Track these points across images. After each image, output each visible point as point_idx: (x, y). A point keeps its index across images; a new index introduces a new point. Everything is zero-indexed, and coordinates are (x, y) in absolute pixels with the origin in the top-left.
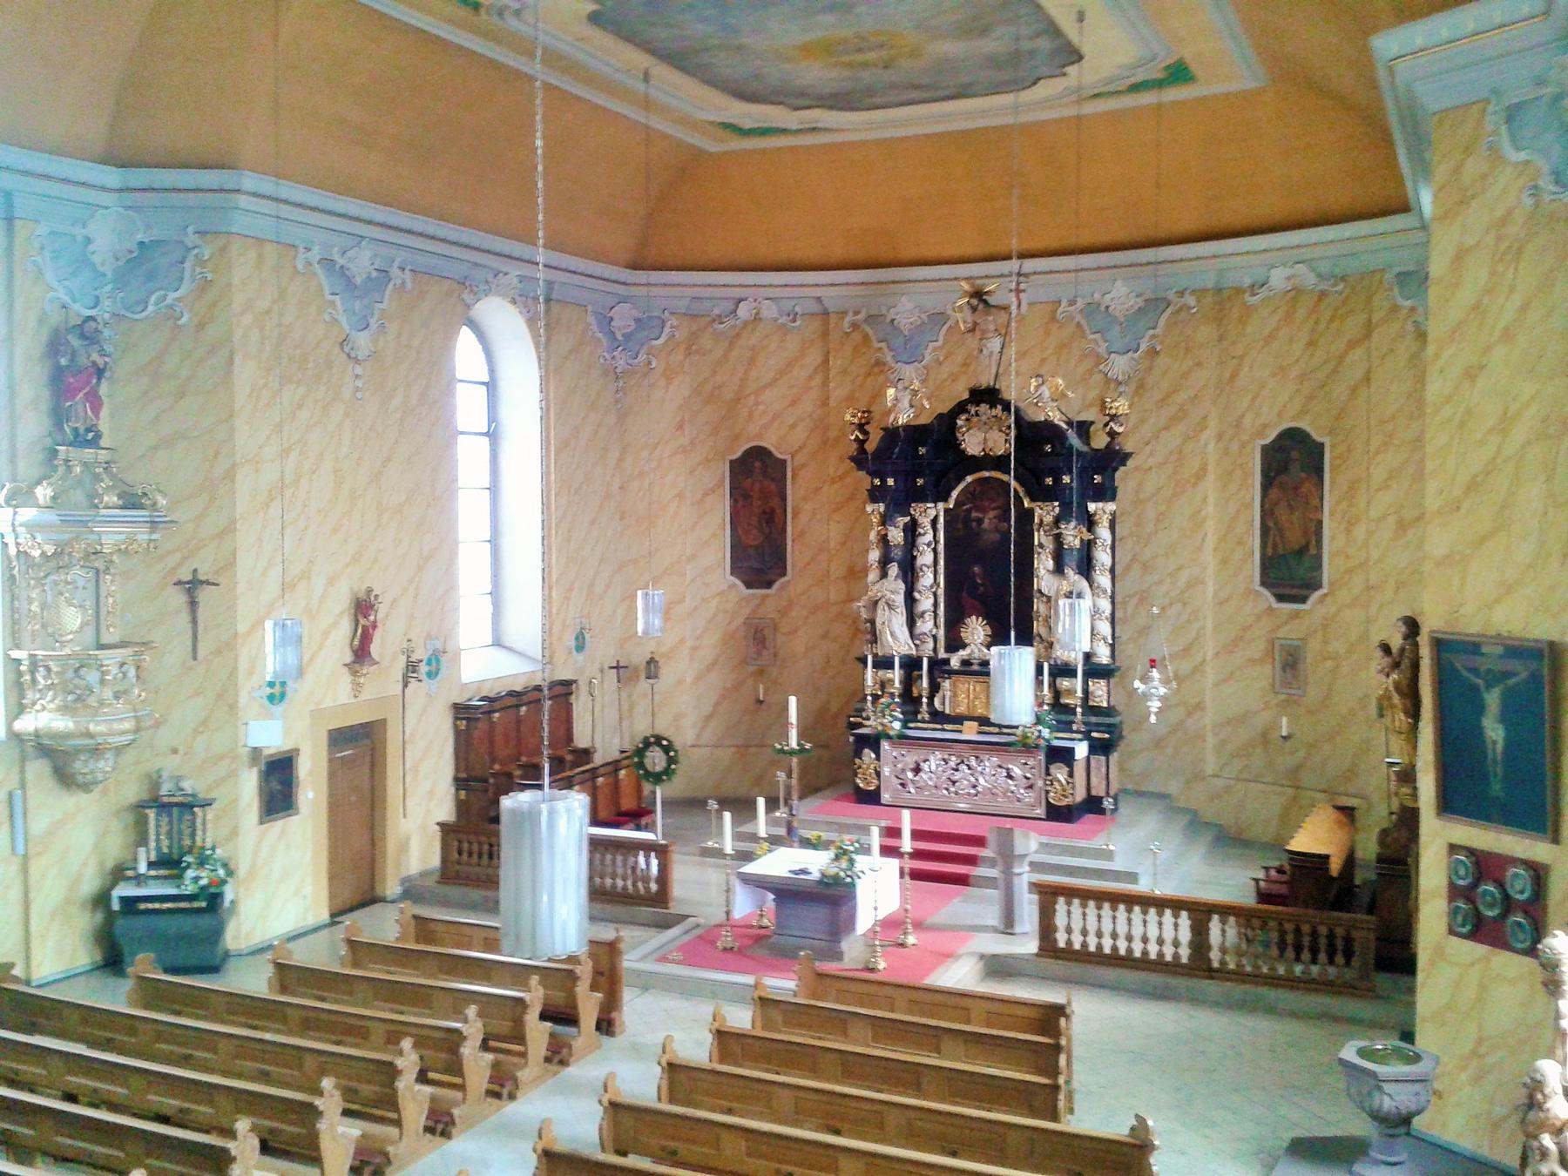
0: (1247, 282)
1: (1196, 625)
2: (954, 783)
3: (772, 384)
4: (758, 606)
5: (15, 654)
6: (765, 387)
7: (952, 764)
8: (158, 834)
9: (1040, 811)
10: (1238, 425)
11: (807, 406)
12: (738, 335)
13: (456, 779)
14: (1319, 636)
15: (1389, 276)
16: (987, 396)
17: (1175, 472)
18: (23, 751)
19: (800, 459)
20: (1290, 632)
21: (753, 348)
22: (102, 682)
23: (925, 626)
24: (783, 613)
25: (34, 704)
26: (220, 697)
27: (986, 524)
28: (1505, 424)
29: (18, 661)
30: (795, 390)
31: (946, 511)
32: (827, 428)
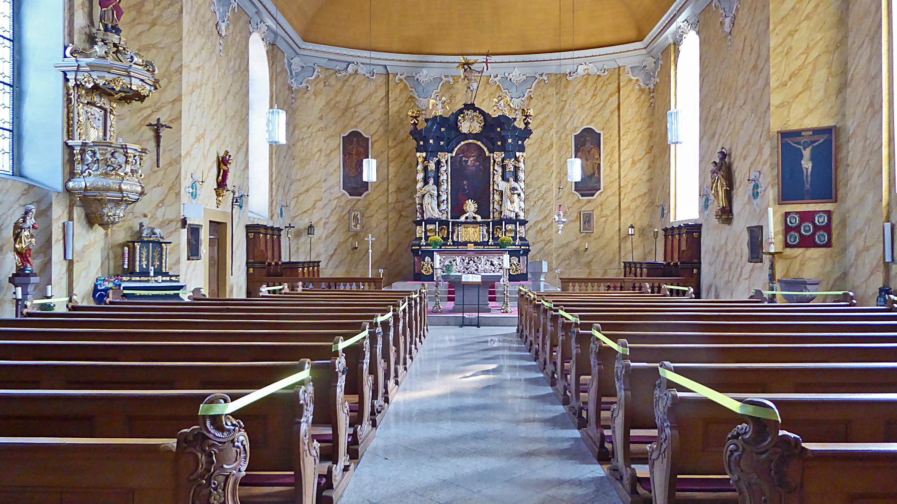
3: (361, 103)
5: (70, 143)
7: (467, 261)
8: (140, 258)
11: (378, 115)
12: (347, 80)
13: (247, 263)
14: (599, 209)
15: (628, 68)
16: (470, 107)
18: (71, 201)
19: (375, 138)
20: (586, 209)
22: (127, 162)
23: (443, 207)
25: (82, 172)
26: (171, 188)
28: (807, 51)
29: (71, 148)
31: (452, 157)
32: (388, 125)
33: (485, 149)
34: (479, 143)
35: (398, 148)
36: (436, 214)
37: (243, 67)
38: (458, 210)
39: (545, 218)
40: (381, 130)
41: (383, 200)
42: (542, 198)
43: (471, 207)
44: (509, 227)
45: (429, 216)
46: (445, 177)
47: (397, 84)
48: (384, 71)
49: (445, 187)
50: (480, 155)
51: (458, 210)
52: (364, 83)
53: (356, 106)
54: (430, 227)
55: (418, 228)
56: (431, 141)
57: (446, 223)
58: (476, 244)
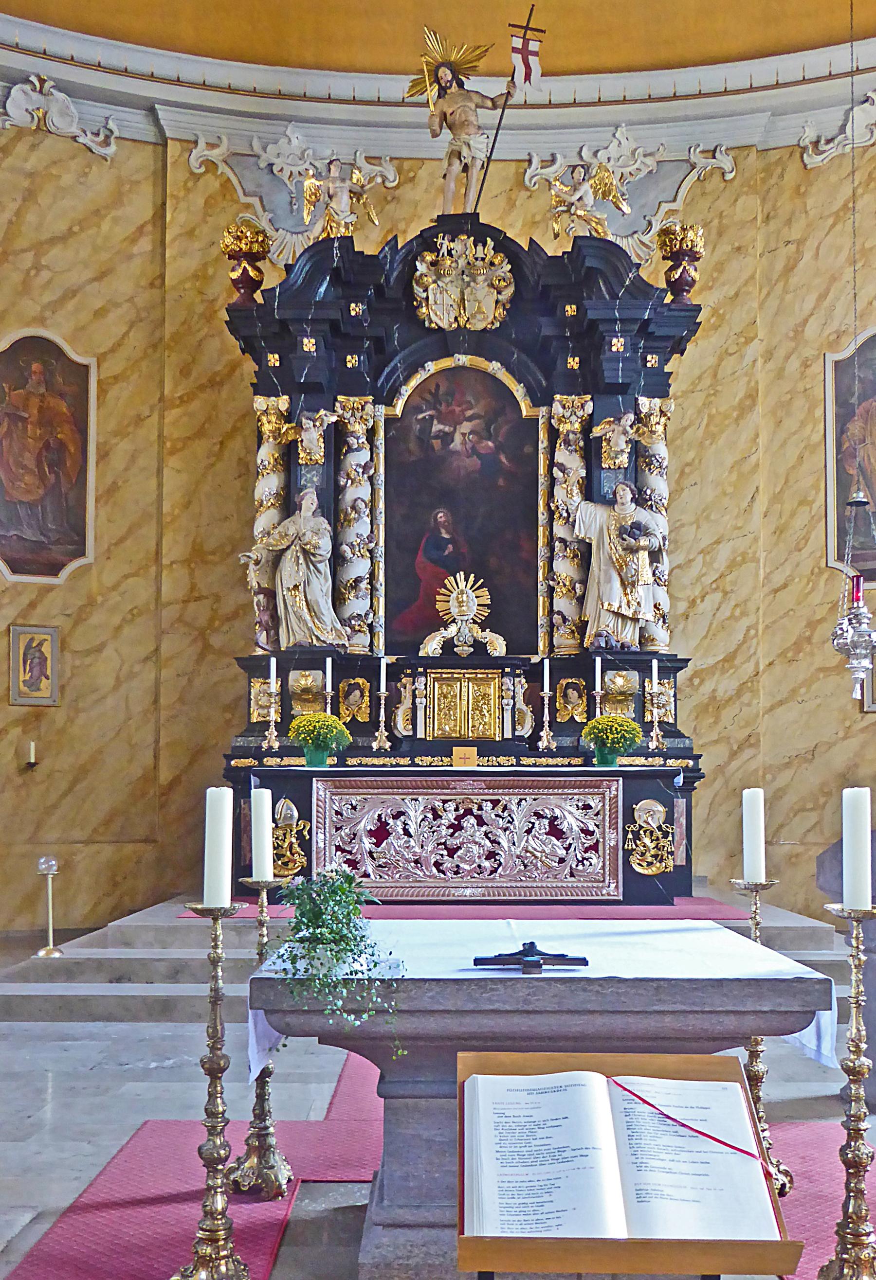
0: (810, 135)
1: (745, 622)
2: (452, 852)
4: (32, 605)
6: (53, 241)
7: (450, 816)
9: (613, 890)
10: (798, 331)
11: (125, 283)
17: (707, 404)
21: (31, 175)
23: (357, 605)
24: (79, 618)
27: (457, 443)
30: (104, 256)
31: (390, 421)
33: (518, 391)
34: (494, 367)
35: (195, 405)
36: (328, 631)
37: (597, 988)
38: (412, 613)
39: (730, 658)
40: (137, 339)
41: (141, 590)
42: (717, 585)
43: (464, 601)
44: (620, 680)
45: (300, 636)
47: (196, 177)
48: (149, 133)
49: (362, 527)
50: (490, 420)
51: (412, 613)
52: (74, 165)
53: (39, 248)
54: (300, 679)
55: (257, 686)
56: (309, 345)
57: (367, 666)
58: (486, 747)
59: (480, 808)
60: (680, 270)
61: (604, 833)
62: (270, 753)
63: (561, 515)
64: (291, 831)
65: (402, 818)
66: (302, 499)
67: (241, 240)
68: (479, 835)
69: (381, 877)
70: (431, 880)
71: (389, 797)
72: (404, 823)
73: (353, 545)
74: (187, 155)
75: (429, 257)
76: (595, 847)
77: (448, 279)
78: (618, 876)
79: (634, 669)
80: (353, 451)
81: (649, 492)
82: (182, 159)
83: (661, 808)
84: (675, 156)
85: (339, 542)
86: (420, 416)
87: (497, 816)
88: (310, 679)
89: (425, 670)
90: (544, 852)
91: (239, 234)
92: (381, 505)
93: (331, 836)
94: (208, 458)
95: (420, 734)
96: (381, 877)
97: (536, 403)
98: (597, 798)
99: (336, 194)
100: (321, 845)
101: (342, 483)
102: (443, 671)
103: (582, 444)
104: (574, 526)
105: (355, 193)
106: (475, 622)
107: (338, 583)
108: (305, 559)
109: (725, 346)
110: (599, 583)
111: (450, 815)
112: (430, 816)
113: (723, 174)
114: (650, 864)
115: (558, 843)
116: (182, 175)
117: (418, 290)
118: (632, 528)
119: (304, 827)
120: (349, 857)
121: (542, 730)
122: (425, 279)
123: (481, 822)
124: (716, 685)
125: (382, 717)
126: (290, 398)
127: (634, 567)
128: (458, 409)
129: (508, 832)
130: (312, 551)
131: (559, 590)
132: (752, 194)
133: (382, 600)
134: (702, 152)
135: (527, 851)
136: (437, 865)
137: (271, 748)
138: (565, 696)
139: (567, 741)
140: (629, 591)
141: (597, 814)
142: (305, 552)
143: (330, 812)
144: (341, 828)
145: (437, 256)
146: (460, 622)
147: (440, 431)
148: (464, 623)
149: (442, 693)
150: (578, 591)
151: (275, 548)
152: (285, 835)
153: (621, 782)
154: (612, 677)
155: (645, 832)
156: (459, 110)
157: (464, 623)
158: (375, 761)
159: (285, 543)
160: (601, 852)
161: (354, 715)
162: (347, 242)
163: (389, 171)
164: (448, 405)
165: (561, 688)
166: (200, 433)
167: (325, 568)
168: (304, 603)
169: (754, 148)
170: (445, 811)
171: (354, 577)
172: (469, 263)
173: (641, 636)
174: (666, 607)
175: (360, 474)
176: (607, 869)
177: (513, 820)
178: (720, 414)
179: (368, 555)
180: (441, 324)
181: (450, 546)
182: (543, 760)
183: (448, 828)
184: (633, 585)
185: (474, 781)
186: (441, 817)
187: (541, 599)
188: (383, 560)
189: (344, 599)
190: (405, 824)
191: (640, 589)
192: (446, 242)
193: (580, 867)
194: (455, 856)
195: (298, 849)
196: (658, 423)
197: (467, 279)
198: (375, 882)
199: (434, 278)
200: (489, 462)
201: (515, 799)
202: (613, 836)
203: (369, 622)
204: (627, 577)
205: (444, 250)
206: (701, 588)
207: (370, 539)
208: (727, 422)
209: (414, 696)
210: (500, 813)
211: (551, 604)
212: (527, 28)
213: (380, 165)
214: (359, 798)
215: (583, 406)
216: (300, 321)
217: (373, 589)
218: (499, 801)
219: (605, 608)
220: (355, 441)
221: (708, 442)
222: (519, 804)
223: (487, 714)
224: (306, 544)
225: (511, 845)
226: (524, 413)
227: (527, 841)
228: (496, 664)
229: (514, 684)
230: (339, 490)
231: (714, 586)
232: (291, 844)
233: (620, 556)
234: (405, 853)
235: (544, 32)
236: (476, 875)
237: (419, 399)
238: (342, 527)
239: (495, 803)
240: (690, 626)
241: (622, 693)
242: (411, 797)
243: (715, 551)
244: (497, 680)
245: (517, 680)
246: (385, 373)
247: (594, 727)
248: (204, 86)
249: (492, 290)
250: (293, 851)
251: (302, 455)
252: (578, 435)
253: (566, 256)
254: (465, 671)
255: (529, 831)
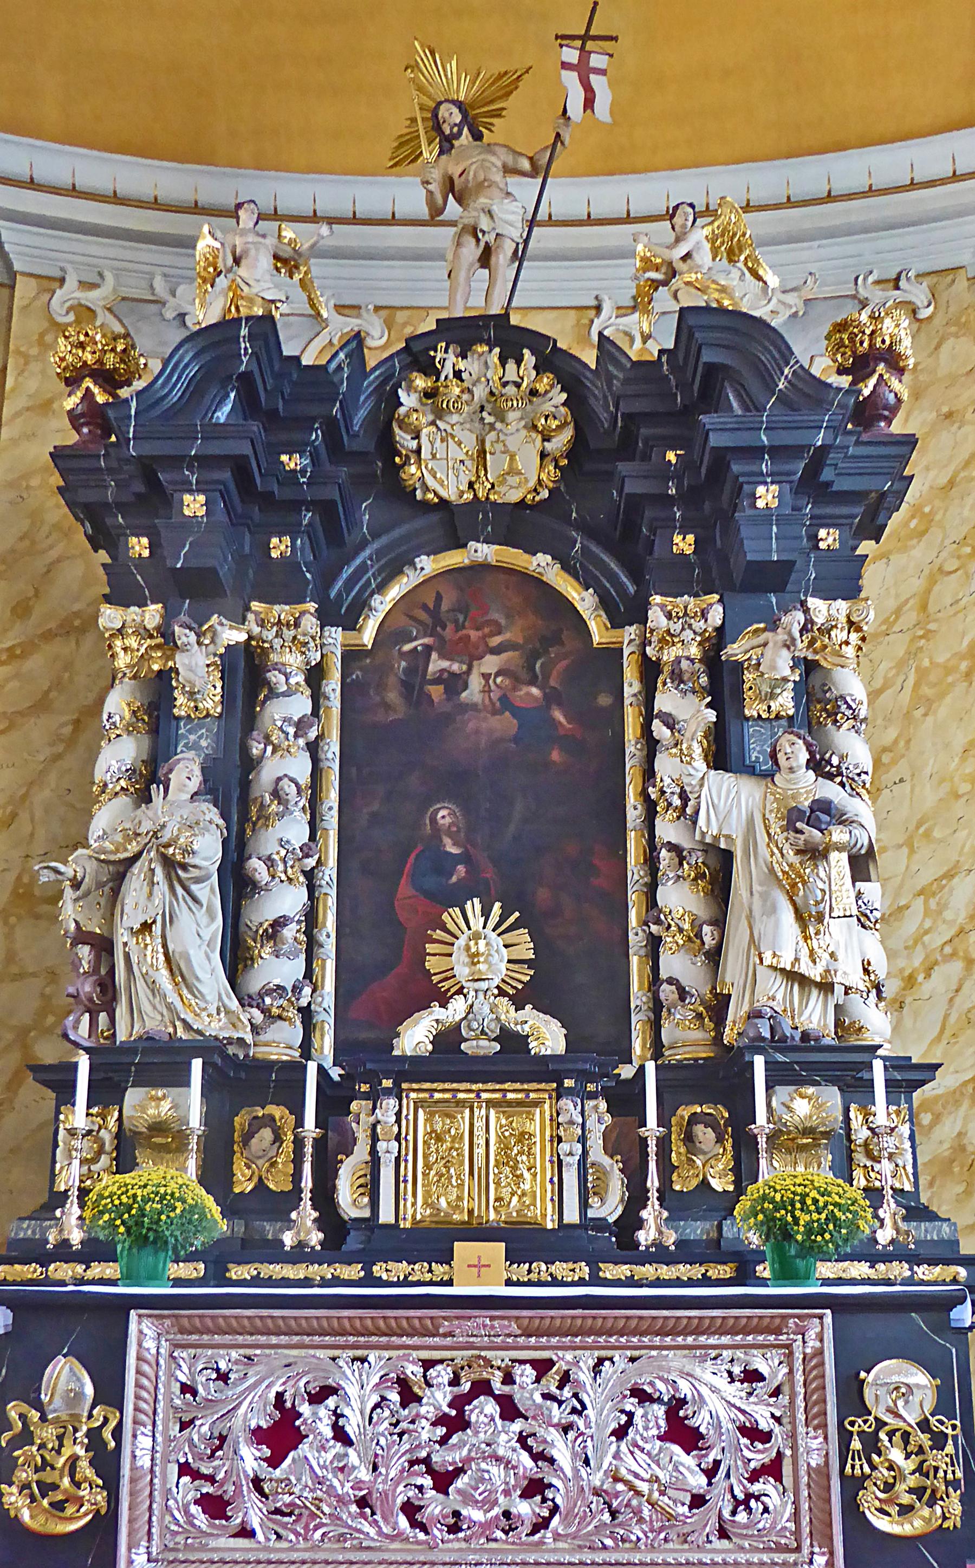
2: (443, 1481)
7: (439, 1399)
17: (913, 653)
23: (277, 969)
27: (474, 691)
31: (351, 656)
33: (584, 601)
34: (541, 564)
35: (35, 663)
36: (211, 1008)
38: (385, 970)
43: (482, 954)
44: (804, 1106)
45: (153, 1022)
46: (299, 767)
51: (385, 970)
57: (284, 1082)
58: (524, 1242)
59: (508, 1379)
60: (872, 381)
61: (793, 1436)
62: (64, 1252)
63: (670, 804)
64: (76, 1430)
65: (331, 1402)
66: (171, 771)
67: (84, 349)
68: (506, 1443)
69: (279, 1537)
70: (396, 1545)
71: (303, 1352)
72: (335, 1412)
73: (273, 861)
74: (47, 296)
75: (421, 382)
76: (773, 1469)
77: (455, 418)
78: (831, 1539)
79: (832, 1081)
80: (278, 696)
81: (835, 761)
82: (38, 303)
83: (920, 1378)
84: (832, 291)
85: (246, 855)
86: (407, 647)
87: (546, 1396)
88: (166, 1106)
89: (397, 1084)
90: (657, 1480)
91: (82, 338)
92: (332, 797)
93: (169, 1440)
94: (52, 744)
95: (386, 1216)
96: (279, 1537)
97: (617, 622)
98: (775, 1356)
99: (246, 252)
100: (145, 1462)
101: (255, 751)
102: (435, 1085)
103: (704, 680)
104: (695, 823)
105: (285, 261)
106: (502, 993)
107: (242, 928)
108: (168, 877)
109: (939, 560)
110: (750, 917)
111: (439, 1395)
112: (394, 1397)
113: (914, 312)
114: (906, 1510)
115: (689, 1460)
116: (36, 325)
117: (404, 440)
118: (812, 811)
119: (106, 1420)
120: (207, 1489)
121: (645, 1207)
122: (415, 416)
123: (510, 1410)
124: (965, 1124)
125: (307, 1182)
126: (164, 607)
127: (821, 885)
128: (474, 635)
129: (571, 1435)
130: (179, 857)
131: (668, 939)
132: (964, 335)
133: (330, 966)
134: (877, 282)
135: (617, 1479)
136: (410, 1509)
137: (66, 1243)
138: (689, 1139)
139: (698, 1230)
140: (812, 930)
141: (776, 1393)
142: (169, 864)
143: (168, 1386)
144: (192, 1422)
145: (437, 380)
146: (472, 993)
147: (442, 671)
148: (481, 995)
149: (433, 1131)
150: (707, 939)
151: (112, 858)
152: (60, 1438)
153: (828, 1320)
154: (786, 1099)
155: (891, 1434)
156: (474, 167)
157: (481, 995)
158: (290, 1272)
159: (133, 848)
160: (788, 1480)
161: (260, 1178)
162: (265, 328)
163: (372, 324)
164: (459, 627)
165: (680, 1124)
166: (41, 705)
167: (209, 892)
168: (162, 958)
169: (962, 271)
170: (429, 1385)
171: (272, 917)
172: (492, 393)
173: (838, 1024)
174: (881, 968)
175: (291, 737)
176: (805, 1521)
177: (584, 1407)
178: (938, 665)
179: (302, 879)
180: (443, 493)
181: (461, 868)
182: (648, 1271)
183: (434, 1424)
184: (820, 918)
185: (492, 1318)
186: (419, 1400)
187: (634, 960)
188: (334, 893)
189: (252, 959)
190: (337, 1415)
191: (835, 926)
192: (451, 358)
193: (742, 1517)
194: (451, 1489)
195: (90, 1473)
196: (847, 643)
197: (489, 419)
198: (267, 1549)
199: (431, 417)
200: (533, 724)
201: (589, 1360)
202: (815, 1444)
203: (304, 1002)
204: (807, 905)
205: (448, 370)
206: (923, 956)
207: (306, 851)
208: (950, 679)
209: (375, 1139)
210: (554, 1390)
211: (655, 968)
212: (585, 38)
213: (358, 316)
214: (234, 1354)
215: (704, 614)
216: (177, 461)
217: (311, 947)
218: (550, 1363)
219: (767, 962)
220: (283, 678)
221: (921, 711)
222: (597, 1369)
223: (527, 1175)
224: (167, 846)
225: (579, 1464)
226: (596, 639)
227: (617, 1456)
228: (546, 1070)
229: (582, 1113)
230: (250, 764)
231: (948, 950)
232: (74, 1459)
233: (791, 865)
234: (336, 1483)
235: (615, 39)
236: (499, 1534)
237: (404, 617)
238: (253, 830)
239: (542, 1367)
240: (908, 1022)
241: (808, 1131)
242: (351, 1353)
243: (946, 889)
244: (547, 1106)
245: (590, 1104)
246: (345, 576)
247: (764, 1198)
248: (73, 192)
249: (534, 435)
250: (78, 1477)
251: (181, 700)
252: (697, 665)
253: (664, 359)
254: (480, 1086)
255: (620, 1433)
